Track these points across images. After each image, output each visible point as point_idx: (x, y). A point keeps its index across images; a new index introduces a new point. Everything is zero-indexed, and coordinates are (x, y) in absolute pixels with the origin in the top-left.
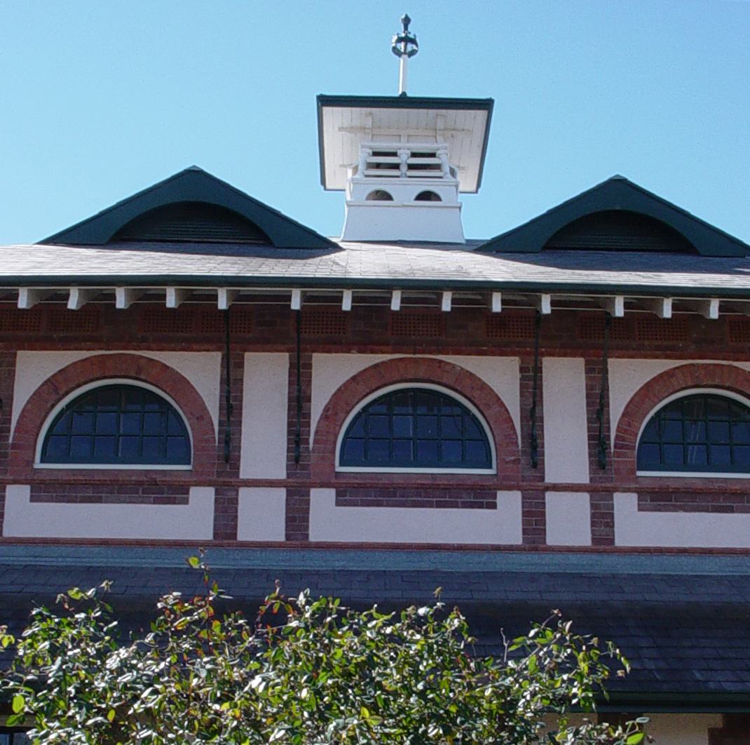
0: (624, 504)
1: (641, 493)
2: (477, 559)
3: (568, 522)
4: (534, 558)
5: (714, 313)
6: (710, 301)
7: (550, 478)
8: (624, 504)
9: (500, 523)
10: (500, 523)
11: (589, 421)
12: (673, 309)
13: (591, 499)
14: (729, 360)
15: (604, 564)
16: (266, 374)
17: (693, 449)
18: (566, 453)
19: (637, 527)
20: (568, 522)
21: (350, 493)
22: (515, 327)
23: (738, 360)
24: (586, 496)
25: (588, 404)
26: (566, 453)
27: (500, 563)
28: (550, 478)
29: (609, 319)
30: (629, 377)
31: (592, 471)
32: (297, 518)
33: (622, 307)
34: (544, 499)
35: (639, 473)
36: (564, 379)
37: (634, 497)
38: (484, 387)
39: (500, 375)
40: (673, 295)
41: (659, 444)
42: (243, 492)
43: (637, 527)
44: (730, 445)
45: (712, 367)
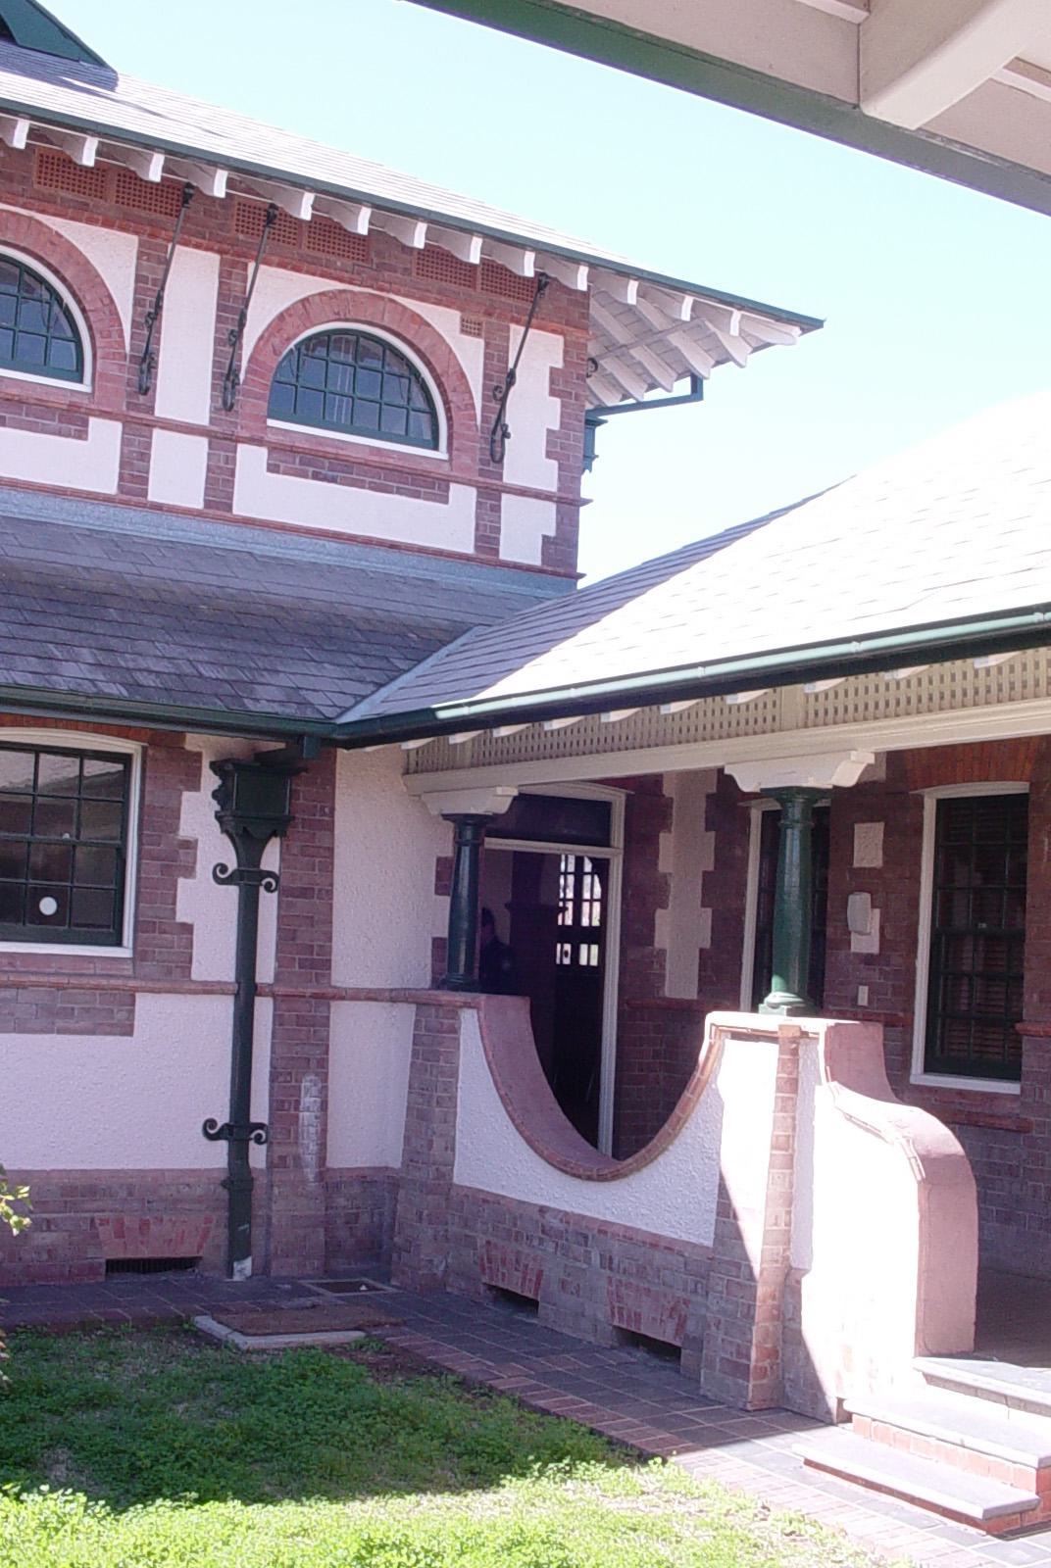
0: (250, 459)
1: (274, 448)
2: (278, 538)
3: (178, 473)
4: (133, 514)
5: (19, 139)
6: (85, 139)
7: (508, 478)
8: (250, 459)
9: (88, 461)
10: (88, 461)
11: (218, 341)
12: (99, 153)
13: (124, 433)
14: (30, 209)
15: (130, 522)
16: (193, 277)
17: (341, 401)
18: (184, 383)
19: (265, 492)
20: (178, 473)
21: (289, 459)
22: (49, 171)
23: (43, 212)
24: (205, 441)
25: (219, 319)
26: (184, 383)
27: (446, 576)
28: (508, 478)
29: (69, 164)
30: (276, 291)
31: (214, 410)
32: (220, 481)
33: (160, 169)
34: (151, 437)
35: (271, 422)
36: (193, 277)
37: (264, 451)
38: (85, 266)
39: (110, 255)
40: (33, 118)
41: (47, 337)
42: (157, 434)
43: (265, 492)
44: (47, 337)
45: (349, 296)
